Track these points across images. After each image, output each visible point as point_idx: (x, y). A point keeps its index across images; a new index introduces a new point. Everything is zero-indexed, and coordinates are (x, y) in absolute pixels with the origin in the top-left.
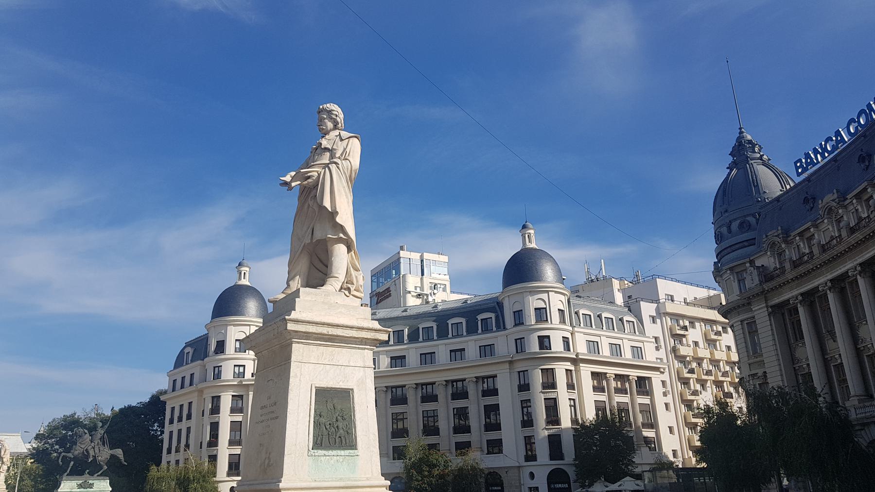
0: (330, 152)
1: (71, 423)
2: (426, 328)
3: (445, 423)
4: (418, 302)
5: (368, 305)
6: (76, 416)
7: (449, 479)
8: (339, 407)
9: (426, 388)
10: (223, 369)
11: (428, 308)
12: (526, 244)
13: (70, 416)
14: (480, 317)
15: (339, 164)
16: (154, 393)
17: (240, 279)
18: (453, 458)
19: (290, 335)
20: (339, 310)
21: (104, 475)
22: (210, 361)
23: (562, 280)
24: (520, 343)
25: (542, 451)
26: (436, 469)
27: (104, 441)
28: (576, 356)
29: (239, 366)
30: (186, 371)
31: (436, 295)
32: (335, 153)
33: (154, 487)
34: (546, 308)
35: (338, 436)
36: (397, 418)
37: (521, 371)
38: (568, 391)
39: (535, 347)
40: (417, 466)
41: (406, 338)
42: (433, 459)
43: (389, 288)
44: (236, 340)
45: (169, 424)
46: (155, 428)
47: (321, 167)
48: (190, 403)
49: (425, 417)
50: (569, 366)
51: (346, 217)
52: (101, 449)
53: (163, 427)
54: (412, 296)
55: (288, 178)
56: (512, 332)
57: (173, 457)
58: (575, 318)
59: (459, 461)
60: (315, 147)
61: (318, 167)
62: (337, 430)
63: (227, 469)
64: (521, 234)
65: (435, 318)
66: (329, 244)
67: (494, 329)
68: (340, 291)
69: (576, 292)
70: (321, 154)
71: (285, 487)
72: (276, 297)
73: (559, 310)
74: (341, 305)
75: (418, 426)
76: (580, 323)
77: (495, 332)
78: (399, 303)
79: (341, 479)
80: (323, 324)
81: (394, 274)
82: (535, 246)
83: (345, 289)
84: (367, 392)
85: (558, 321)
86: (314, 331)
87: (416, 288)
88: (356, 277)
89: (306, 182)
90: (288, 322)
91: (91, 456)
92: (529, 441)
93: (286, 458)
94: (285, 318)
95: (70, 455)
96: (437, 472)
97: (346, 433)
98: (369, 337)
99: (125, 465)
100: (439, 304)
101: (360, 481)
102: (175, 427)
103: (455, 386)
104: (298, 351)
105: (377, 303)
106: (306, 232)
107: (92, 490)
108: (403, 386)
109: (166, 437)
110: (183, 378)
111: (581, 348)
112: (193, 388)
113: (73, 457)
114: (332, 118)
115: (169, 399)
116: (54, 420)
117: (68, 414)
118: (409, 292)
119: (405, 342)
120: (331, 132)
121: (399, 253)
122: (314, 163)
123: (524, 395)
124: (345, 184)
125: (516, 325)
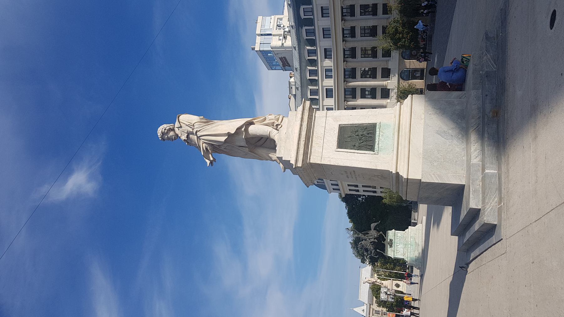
0: (189, 134)
1: (356, 243)
3: (369, 21)
4: (289, 38)
5: (290, 73)
6: (352, 242)
7: (405, 20)
8: (350, 134)
9: (346, 34)
11: (293, 32)
13: (352, 245)
15: (197, 130)
20: (290, 132)
21: (385, 233)
26: (399, 29)
27: (366, 234)
31: (285, 25)
32: (190, 131)
35: (368, 135)
40: (396, 42)
41: (313, 48)
42: (391, 30)
43: (280, 58)
49: (365, 35)
52: (370, 235)
53: (361, 195)
54: (285, 42)
55: (208, 162)
60: (186, 143)
65: (300, 28)
66: (248, 137)
68: (278, 130)
70: (191, 140)
71: (395, 170)
72: (282, 168)
74: (287, 131)
75: (371, 40)
78: (288, 51)
79: (393, 134)
80: (298, 144)
81: (270, 54)
83: (277, 127)
84: (342, 115)
87: (280, 40)
88: (270, 120)
89: (210, 151)
90: (297, 166)
91: (374, 240)
94: (295, 168)
95: (373, 251)
96: (401, 29)
98: (308, 114)
99: (380, 222)
100: (290, 24)
101: (395, 122)
103: (346, 14)
104: (315, 159)
105: (290, 66)
107: (393, 240)
108: (344, 50)
112: (340, 184)
113: (374, 250)
114: (167, 132)
115: (344, 191)
116: (354, 253)
117: (350, 246)
118: (283, 44)
119: (315, 48)
120: (177, 133)
121: (257, 51)
122: (197, 144)
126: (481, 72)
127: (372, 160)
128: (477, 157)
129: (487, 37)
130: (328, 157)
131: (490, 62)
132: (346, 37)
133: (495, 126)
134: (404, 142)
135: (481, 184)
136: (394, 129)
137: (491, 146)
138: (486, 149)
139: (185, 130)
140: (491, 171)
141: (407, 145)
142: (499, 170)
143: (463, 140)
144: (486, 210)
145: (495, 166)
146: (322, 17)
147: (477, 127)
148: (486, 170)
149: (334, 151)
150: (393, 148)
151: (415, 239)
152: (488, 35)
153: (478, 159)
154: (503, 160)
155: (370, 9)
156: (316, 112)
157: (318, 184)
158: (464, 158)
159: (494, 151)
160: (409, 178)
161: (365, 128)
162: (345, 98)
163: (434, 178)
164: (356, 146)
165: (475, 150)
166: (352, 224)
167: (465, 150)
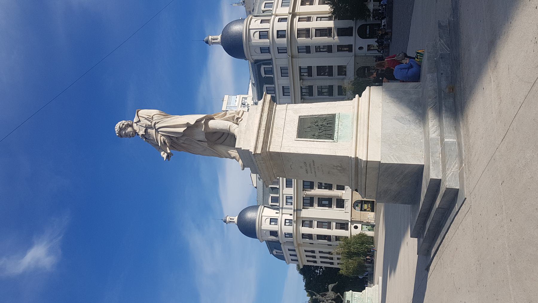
2: (267, 91)
8: (310, 125)
10: (287, 232)
12: (218, 42)
14: (263, 75)
15: (156, 122)
16: (298, 272)
17: (234, 222)
18: (347, 97)
19: (264, 152)
21: (343, 295)
22: (281, 239)
23: (243, 20)
24: (281, 50)
25: (347, 40)
27: (324, 295)
28: (290, 14)
29: (285, 222)
30: (286, 253)
31: (249, 103)
32: (148, 125)
33: (351, 272)
34: (260, 32)
35: (327, 125)
36: (320, 93)
37: (298, 50)
38: (311, 21)
39: (284, 41)
44: (270, 224)
45: (315, 253)
46: (319, 272)
47: (157, 134)
48: (305, 251)
50: (296, 19)
51: (192, 119)
52: (328, 296)
55: (164, 156)
56: (273, 55)
57: (335, 261)
58: (267, 13)
59: (349, 93)
60: (144, 139)
61: (158, 136)
62: (323, 126)
63: (344, 230)
64: (212, 45)
66: (208, 131)
67: (271, 66)
68: (238, 125)
69: (250, 12)
71: (354, 154)
73: (261, 23)
74: (247, 123)
76: (270, 10)
77: (273, 66)
79: (352, 123)
82: (220, 36)
83: (237, 121)
85: (268, 24)
86: (262, 138)
88: (230, 114)
89: (167, 144)
91: (332, 301)
92: (340, 48)
93: (338, 155)
97: (325, 120)
98: (268, 106)
100: (254, 101)
101: (354, 112)
102: (318, 260)
103: (305, 94)
104: (274, 147)
106: (200, 145)
107: (351, 301)
109: (324, 265)
110: (291, 255)
111: (285, 11)
112: (298, 255)
123: (313, 50)
124: (169, 119)
125: (269, 52)
126: (435, 59)
127: (331, 148)
128: (435, 132)
129: (440, 26)
130: (288, 146)
131: (444, 46)
132: (304, 95)
133: (451, 100)
134: (362, 128)
135: (440, 157)
136: (353, 118)
137: (449, 117)
138: (444, 120)
139: (144, 124)
140: (450, 139)
141: (366, 131)
142: (458, 139)
143: (420, 124)
144: (447, 175)
145: (454, 135)
146: (283, 96)
147: (434, 106)
148: (446, 139)
149: (294, 140)
150: (353, 135)
151: (371, 300)
152: (440, 24)
153: (436, 134)
154: (461, 125)
155: (326, 90)
156: (276, 106)
157: (277, 254)
158: (422, 141)
159: (452, 121)
160: (368, 160)
161: (324, 119)
162: (303, 188)
163: (393, 159)
164: (316, 135)
165: (433, 126)
166: (310, 297)
167: (422, 134)
